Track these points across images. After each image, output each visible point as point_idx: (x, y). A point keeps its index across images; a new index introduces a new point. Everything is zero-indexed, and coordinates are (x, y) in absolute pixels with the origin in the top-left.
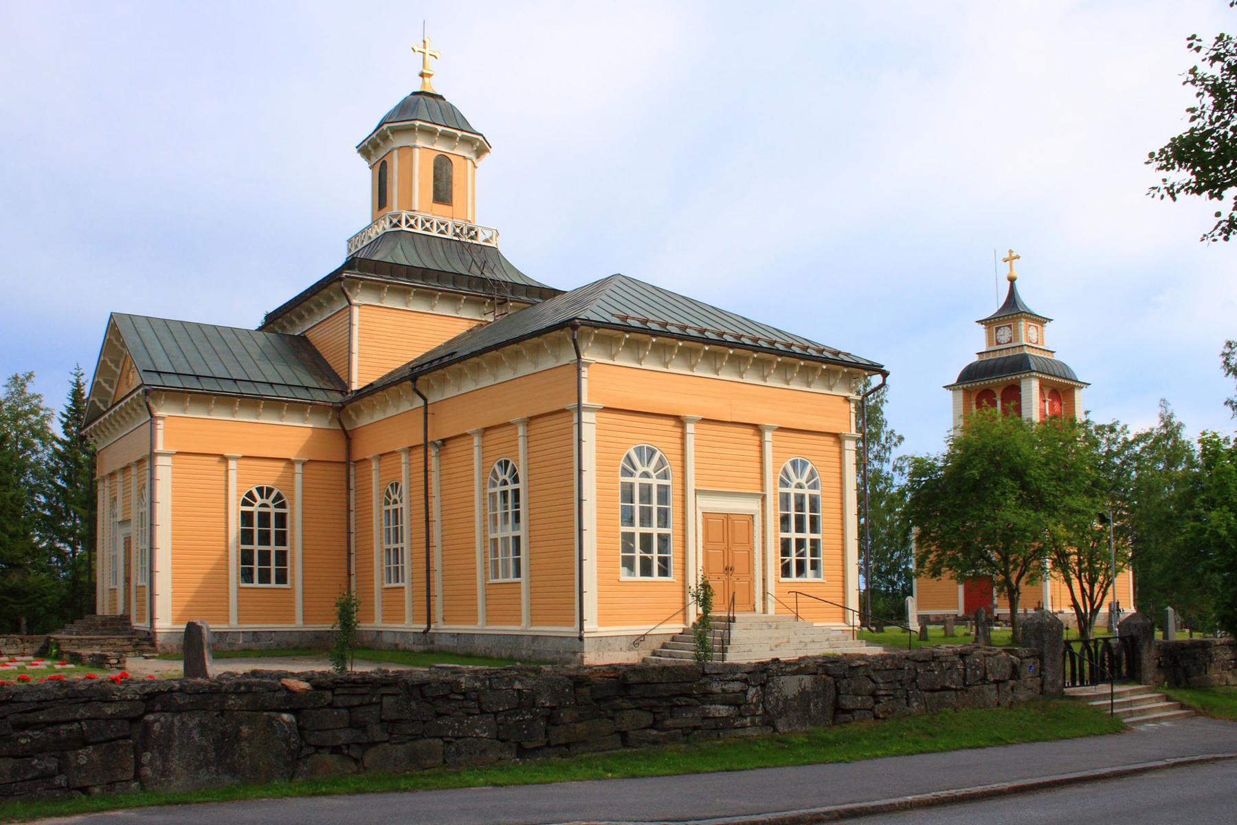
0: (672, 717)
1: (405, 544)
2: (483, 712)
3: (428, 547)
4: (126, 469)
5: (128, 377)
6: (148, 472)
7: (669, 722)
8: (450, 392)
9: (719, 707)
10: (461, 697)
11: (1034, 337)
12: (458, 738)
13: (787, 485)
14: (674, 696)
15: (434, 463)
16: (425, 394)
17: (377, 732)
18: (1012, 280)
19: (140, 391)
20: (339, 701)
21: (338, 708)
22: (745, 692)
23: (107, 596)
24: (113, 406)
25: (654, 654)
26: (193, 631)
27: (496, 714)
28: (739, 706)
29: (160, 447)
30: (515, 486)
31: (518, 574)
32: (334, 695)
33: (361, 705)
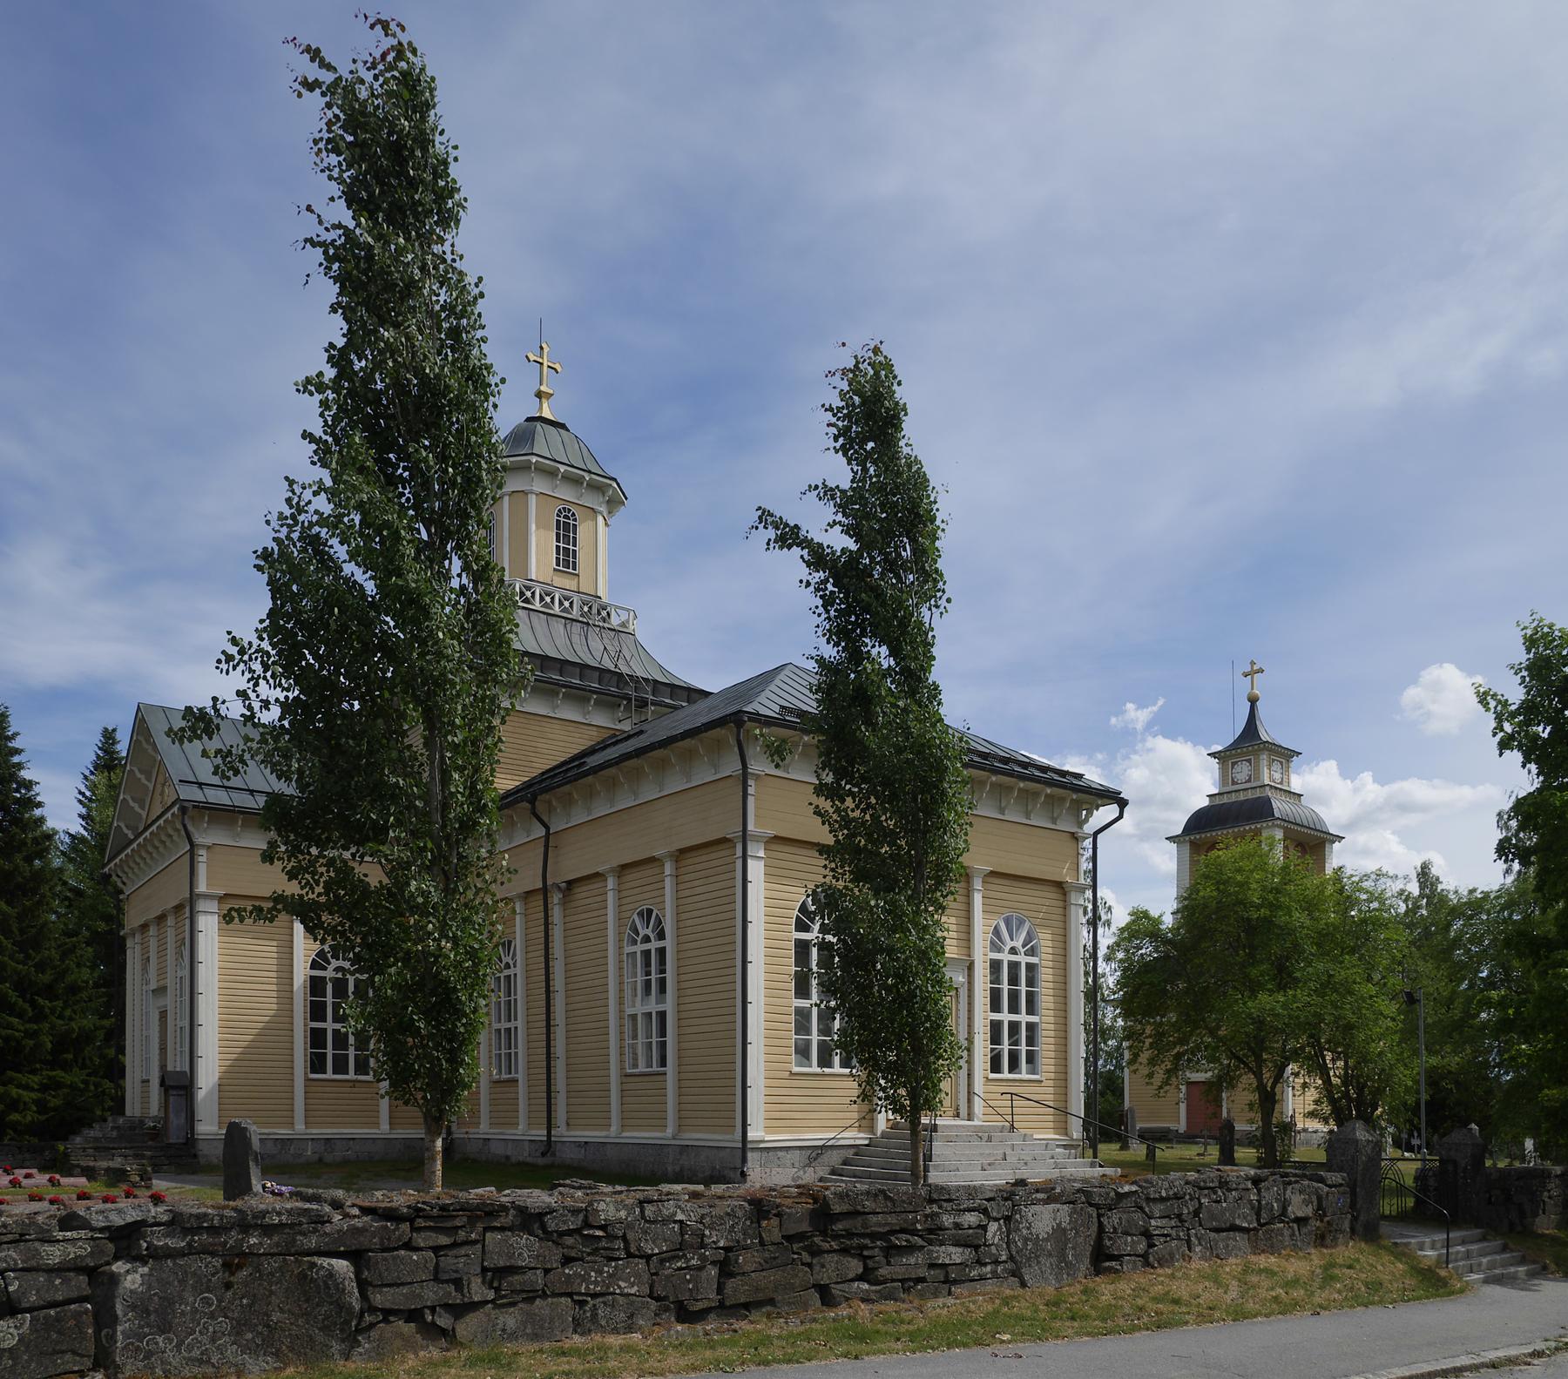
0: (889, 1263)
1: (520, 1023)
2: (630, 1255)
3: (548, 1026)
4: (161, 918)
5: (162, 794)
6: (187, 922)
7: (884, 1271)
8: (579, 817)
9: (952, 1249)
10: (599, 1233)
11: (1277, 776)
12: (595, 1296)
13: (999, 950)
14: (893, 1232)
15: (556, 914)
16: (546, 819)
17: (478, 1290)
18: (1253, 701)
19: (175, 809)
20: (420, 1240)
21: (417, 1249)
22: (984, 1228)
23: (138, 1085)
24: (146, 829)
25: (833, 1172)
26: (236, 1135)
27: (648, 1258)
28: (976, 1248)
29: (202, 887)
30: (660, 944)
31: (663, 1063)
32: (413, 1229)
33: (455, 1245)
